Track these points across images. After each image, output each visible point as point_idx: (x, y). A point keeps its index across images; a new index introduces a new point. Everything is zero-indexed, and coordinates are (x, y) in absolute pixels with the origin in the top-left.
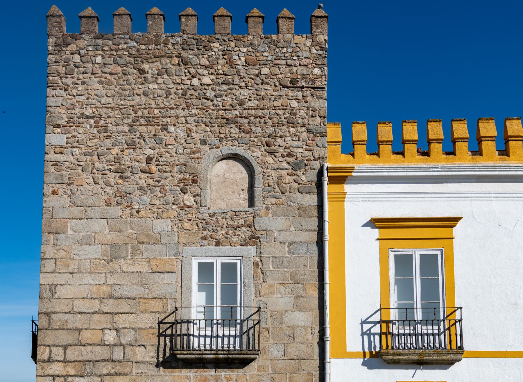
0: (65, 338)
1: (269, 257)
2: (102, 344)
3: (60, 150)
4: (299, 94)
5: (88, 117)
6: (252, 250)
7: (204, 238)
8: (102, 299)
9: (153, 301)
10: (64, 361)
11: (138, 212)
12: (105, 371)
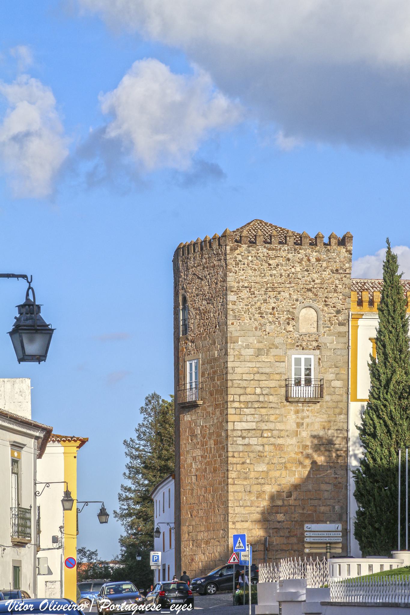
0: (240, 391)
2: (255, 394)
3: (234, 303)
4: (339, 277)
5: (246, 287)
6: (318, 352)
7: (298, 346)
8: (254, 374)
9: (276, 375)
10: (239, 402)
11: (269, 333)
12: (256, 406)
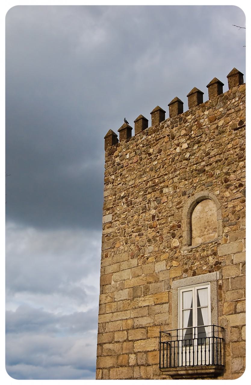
1: (229, 279)
